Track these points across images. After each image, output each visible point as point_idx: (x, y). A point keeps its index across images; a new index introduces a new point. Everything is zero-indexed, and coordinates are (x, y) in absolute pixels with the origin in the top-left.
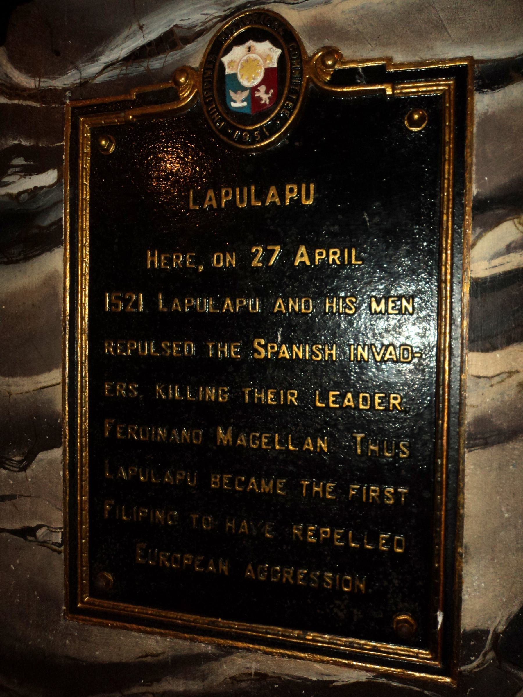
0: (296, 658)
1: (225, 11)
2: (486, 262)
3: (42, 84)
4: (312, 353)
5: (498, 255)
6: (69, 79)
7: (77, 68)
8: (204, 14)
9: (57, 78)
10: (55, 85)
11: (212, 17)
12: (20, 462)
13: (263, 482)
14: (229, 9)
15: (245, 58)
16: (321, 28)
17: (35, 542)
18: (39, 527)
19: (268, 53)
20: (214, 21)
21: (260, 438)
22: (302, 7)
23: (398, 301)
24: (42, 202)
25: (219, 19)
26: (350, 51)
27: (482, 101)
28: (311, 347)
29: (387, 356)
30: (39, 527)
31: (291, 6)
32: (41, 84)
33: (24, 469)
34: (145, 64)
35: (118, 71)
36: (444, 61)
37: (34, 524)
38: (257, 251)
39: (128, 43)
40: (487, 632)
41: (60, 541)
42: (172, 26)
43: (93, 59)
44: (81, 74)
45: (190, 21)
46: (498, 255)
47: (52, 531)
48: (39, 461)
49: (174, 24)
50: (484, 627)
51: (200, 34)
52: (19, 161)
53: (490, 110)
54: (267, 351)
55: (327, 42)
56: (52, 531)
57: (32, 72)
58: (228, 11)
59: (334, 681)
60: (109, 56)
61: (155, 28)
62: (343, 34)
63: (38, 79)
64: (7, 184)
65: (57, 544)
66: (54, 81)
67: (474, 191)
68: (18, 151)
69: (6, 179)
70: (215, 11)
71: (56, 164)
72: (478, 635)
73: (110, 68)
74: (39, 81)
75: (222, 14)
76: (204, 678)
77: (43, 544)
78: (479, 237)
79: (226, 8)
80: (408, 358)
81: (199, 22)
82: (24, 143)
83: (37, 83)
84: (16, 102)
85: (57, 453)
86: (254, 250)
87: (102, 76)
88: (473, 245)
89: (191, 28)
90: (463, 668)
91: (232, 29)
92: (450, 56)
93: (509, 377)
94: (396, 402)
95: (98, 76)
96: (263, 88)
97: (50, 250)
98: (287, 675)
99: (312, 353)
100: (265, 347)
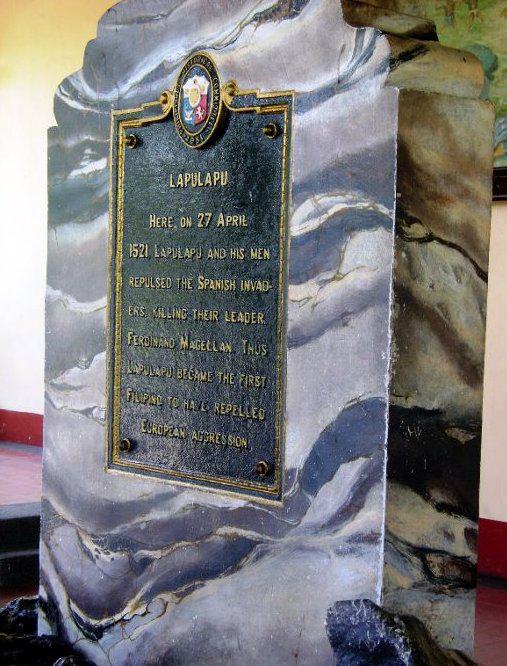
0: (213, 493)
5: (304, 221)
6: (111, 96)
7: (117, 87)
16: (231, 67)
24: (100, 181)
33: (87, 367)
43: (125, 81)
46: (304, 221)
48: (418, 16)
51: (175, 67)
57: (93, 86)
62: (243, 74)
64: (82, 167)
68: (88, 143)
69: (82, 163)
71: (105, 154)
72: (292, 471)
76: (169, 509)
77: (96, 419)
82: (91, 139)
96: (199, 109)
97: (102, 214)
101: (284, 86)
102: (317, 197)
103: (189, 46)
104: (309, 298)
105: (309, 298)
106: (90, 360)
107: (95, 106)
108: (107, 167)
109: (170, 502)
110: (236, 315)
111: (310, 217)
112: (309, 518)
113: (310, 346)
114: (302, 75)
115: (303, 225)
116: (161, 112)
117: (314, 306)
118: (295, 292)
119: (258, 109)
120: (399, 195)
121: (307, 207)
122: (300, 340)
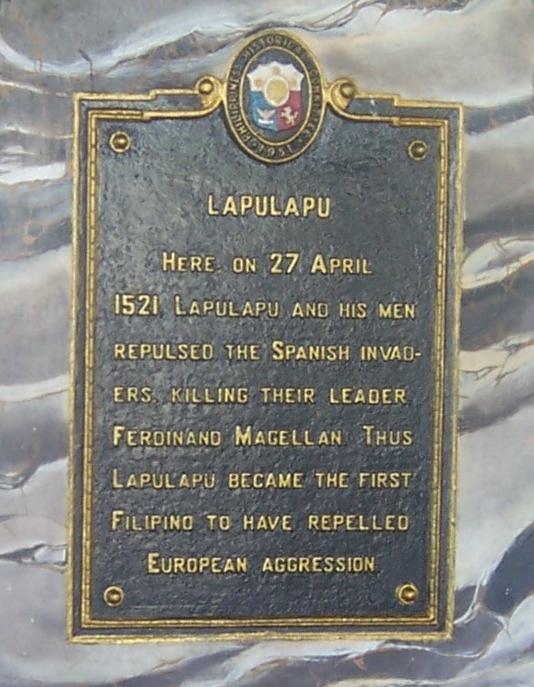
3: (44, 70)
4: (327, 353)
11: (233, 30)
12: (14, 478)
13: (281, 476)
16: (339, 60)
18: (37, 547)
20: (238, 34)
21: (278, 436)
28: (326, 348)
30: (37, 547)
36: (443, 103)
38: (276, 258)
39: (145, 41)
40: (474, 587)
44: (91, 64)
46: (482, 270)
49: (194, 29)
50: (472, 584)
52: (19, 150)
54: (285, 353)
55: (344, 73)
56: (53, 549)
68: (15, 138)
72: (468, 591)
73: (125, 64)
74: (41, 66)
75: (246, 29)
78: (467, 256)
79: (250, 23)
82: (22, 130)
83: (38, 68)
84: (11, 84)
85: (63, 465)
86: (273, 256)
89: (213, 37)
91: (314, 73)
93: (490, 371)
94: (401, 396)
96: (288, 110)
99: (327, 353)
100: (283, 348)
101: (443, 97)
102: (503, 241)
103: (251, 19)
104: (491, 369)
105: (491, 369)
106: (27, 475)
107: (33, 83)
108: (67, 176)
109: (225, 664)
110: (402, 309)
111: (491, 266)
112: (497, 646)
113: (495, 430)
114: (468, 84)
115: (480, 276)
116: (201, 107)
117: (499, 378)
118: (468, 361)
119: (395, 120)
120: (283, 115)
121: (488, 251)
122: (475, 420)
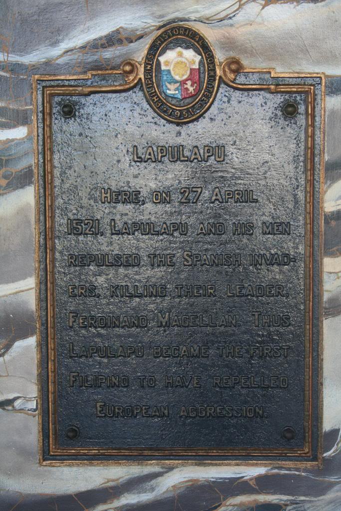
1: (159, 22)
2: (334, 202)
3: (10, 59)
8: (143, 22)
9: (24, 55)
10: (22, 61)
11: (149, 25)
14: (162, 21)
15: (176, 60)
16: (229, 44)
17: (13, 410)
19: (191, 58)
22: (214, 26)
23: (280, 226)
25: (155, 27)
26: (247, 62)
27: (330, 102)
29: (274, 261)
31: (207, 25)
32: (9, 59)
34: (99, 54)
35: (76, 56)
37: (11, 396)
41: (35, 407)
42: (118, 27)
45: (132, 26)
47: (28, 401)
49: (120, 26)
53: (335, 108)
58: (161, 23)
59: (243, 477)
60: (67, 44)
61: (102, 28)
62: (244, 50)
63: (6, 54)
65: (32, 410)
66: (21, 58)
67: (326, 158)
70: (152, 21)
74: (8, 56)
75: (158, 24)
77: (21, 410)
80: (287, 262)
81: (140, 27)
83: (6, 58)
85: (32, 341)
87: (63, 58)
88: (325, 192)
90: (325, 455)
92: (311, 71)
95: (59, 59)
96: (189, 83)
98: (212, 478)
